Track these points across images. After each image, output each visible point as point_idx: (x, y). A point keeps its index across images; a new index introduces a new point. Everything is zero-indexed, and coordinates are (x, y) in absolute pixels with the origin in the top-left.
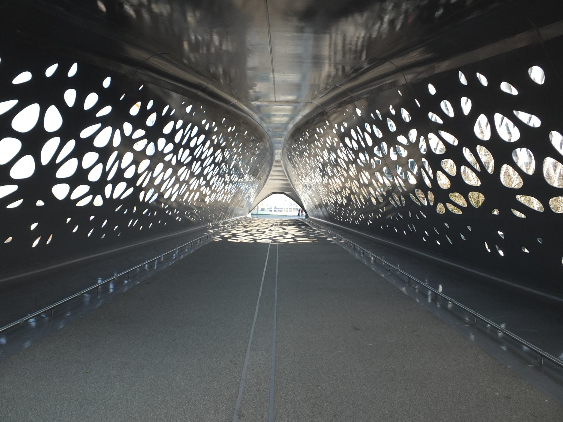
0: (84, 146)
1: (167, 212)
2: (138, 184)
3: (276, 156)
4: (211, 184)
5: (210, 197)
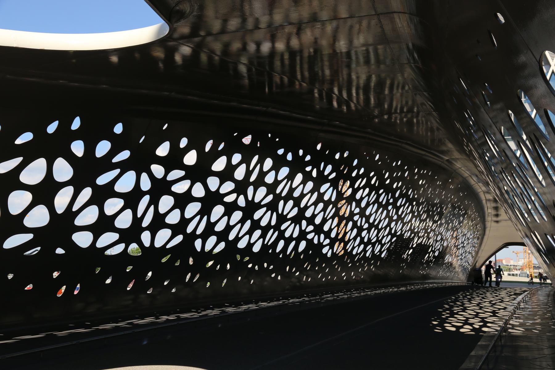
0: (101, 195)
2: (278, 191)
4: (368, 213)
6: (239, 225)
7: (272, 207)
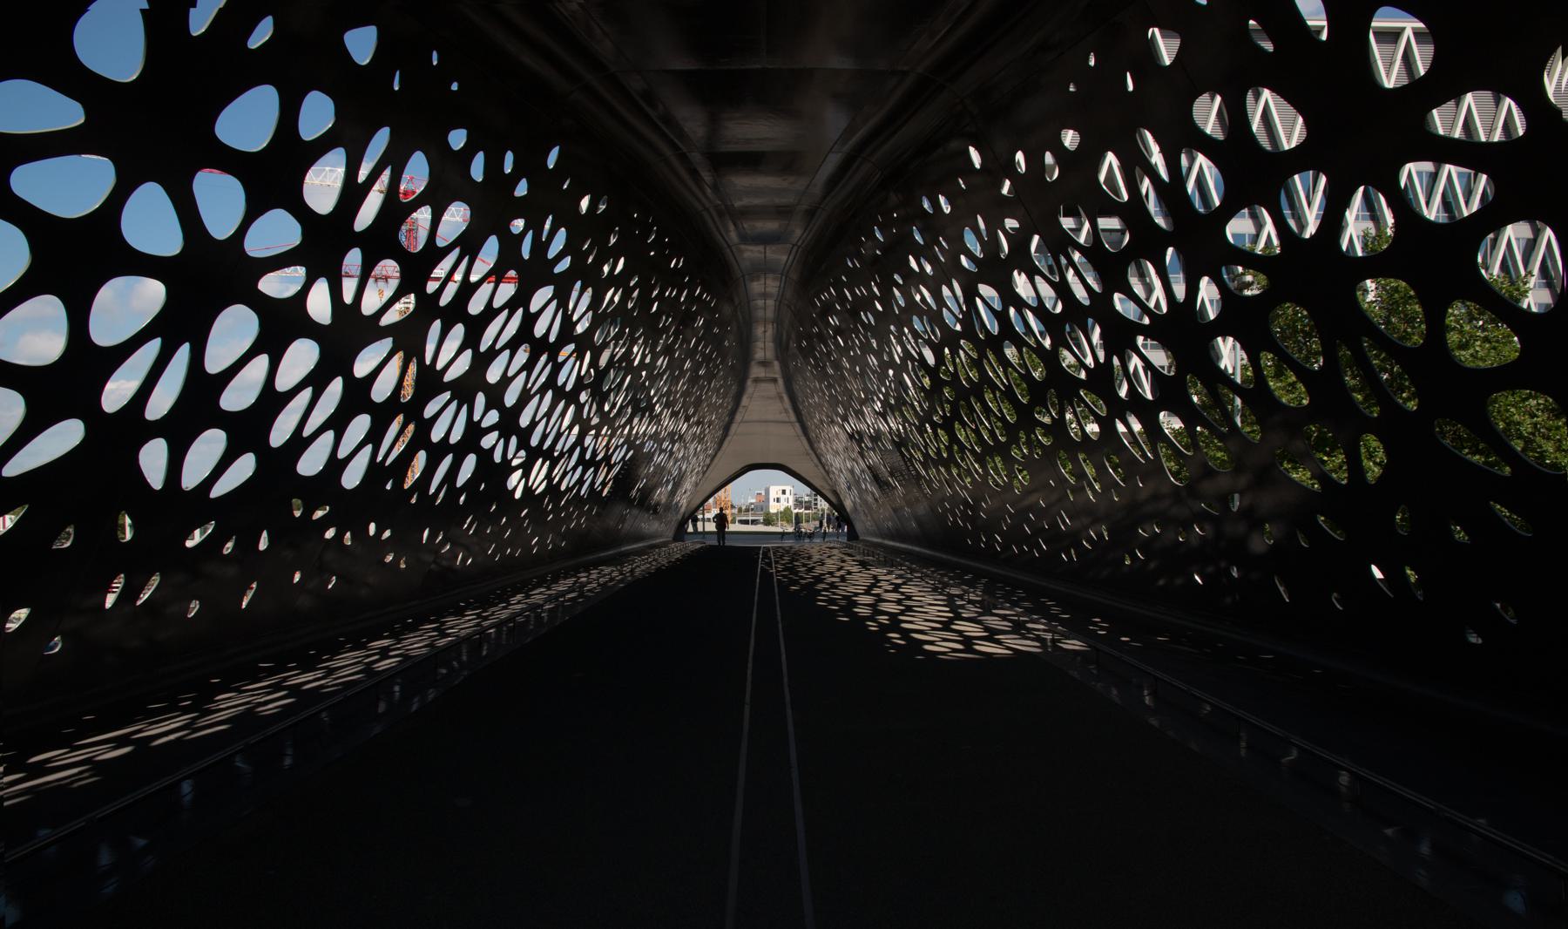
1: (387, 534)
3: (760, 344)
4: (524, 421)
5: (526, 475)
6: (307, 394)
7: (408, 338)
